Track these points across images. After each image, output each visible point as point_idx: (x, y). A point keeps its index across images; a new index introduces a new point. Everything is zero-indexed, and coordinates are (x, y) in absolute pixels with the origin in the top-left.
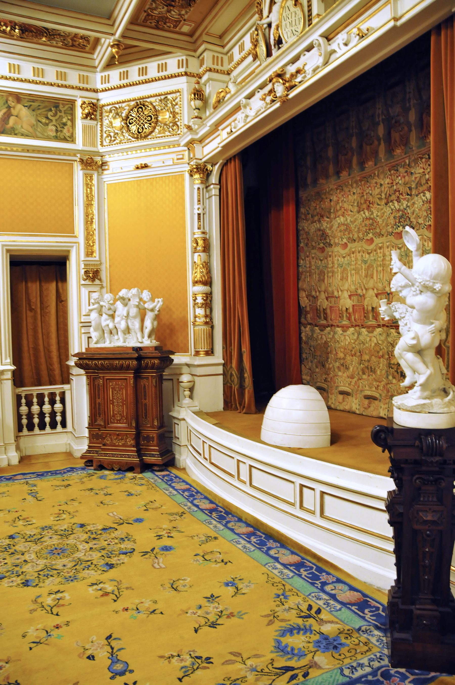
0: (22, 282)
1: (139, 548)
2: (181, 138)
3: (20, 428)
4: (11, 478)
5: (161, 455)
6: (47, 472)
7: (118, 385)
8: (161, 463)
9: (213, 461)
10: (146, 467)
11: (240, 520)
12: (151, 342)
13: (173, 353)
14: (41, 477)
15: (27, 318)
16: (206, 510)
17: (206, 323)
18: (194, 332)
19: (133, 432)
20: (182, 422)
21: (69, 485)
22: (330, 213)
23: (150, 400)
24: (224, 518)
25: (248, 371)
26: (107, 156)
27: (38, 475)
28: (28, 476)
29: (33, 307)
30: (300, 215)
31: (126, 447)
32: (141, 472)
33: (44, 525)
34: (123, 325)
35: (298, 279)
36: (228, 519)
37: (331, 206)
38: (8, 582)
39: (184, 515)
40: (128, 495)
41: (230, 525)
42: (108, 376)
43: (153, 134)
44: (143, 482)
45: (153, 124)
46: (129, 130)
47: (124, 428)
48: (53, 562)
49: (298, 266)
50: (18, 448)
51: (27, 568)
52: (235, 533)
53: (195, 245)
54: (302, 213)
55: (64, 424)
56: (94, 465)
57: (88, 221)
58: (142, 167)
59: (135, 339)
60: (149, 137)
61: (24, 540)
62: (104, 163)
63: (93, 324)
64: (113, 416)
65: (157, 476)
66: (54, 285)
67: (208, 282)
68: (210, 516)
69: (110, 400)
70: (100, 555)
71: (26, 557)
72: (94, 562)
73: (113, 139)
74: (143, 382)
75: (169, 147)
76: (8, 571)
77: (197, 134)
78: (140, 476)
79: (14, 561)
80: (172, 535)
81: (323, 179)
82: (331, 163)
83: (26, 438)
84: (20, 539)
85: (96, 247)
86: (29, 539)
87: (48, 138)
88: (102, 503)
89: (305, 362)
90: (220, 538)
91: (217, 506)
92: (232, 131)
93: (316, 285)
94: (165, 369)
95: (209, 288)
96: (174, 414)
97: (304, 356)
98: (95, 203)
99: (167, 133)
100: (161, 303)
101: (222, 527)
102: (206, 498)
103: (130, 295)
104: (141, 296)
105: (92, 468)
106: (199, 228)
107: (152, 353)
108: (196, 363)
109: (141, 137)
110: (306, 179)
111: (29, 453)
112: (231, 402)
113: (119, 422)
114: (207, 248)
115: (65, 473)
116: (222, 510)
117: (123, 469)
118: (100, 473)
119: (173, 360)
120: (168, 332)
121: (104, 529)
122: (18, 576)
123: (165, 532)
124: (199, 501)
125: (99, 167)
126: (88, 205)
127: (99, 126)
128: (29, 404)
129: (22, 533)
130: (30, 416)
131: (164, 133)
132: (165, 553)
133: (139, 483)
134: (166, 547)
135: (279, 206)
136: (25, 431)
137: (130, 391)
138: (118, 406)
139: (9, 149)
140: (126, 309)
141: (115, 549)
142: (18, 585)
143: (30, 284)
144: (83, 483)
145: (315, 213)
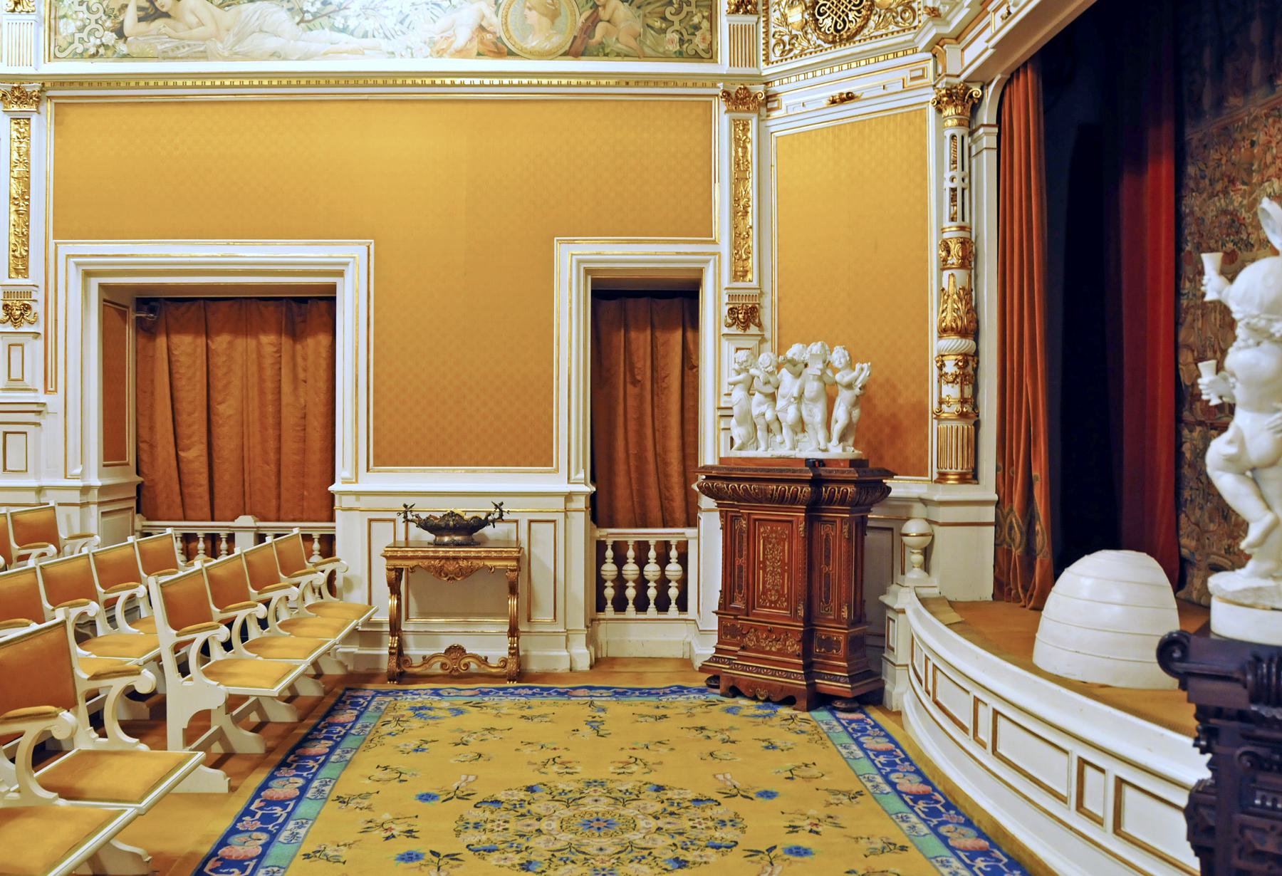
0: (619, 330)
1: (746, 842)
2: (917, 35)
3: (600, 605)
4: (566, 693)
5: (852, 679)
6: (634, 690)
7: (776, 532)
8: (850, 696)
9: (939, 698)
10: (820, 700)
11: (969, 823)
12: (844, 450)
13: (890, 475)
14: (623, 698)
15: (627, 397)
16: (907, 794)
17: (962, 415)
18: (941, 432)
19: (799, 627)
20: (901, 616)
21: (665, 716)
22: (1250, 172)
23: (836, 567)
24: (939, 814)
25: (1042, 518)
26: (777, 83)
27: (616, 693)
28: (597, 693)
29: (639, 378)
30: (1186, 181)
31: (784, 655)
32: (809, 710)
33: (593, 778)
34: (790, 415)
35: (1177, 324)
36: (945, 818)
37: (1253, 156)
38: (499, 860)
39: (860, 798)
40: (767, 748)
41: (943, 830)
42: (757, 514)
43: (865, 31)
44: (806, 727)
45: (864, 12)
46: (818, 27)
47: (783, 617)
48: (585, 841)
49: (1178, 293)
50: (591, 640)
51: (538, 843)
52: (948, 846)
53: (944, 254)
54: (1191, 178)
55: (683, 606)
56: (722, 685)
57: (739, 210)
58: (843, 101)
59: (814, 444)
60: (858, 38)
61: (550, 797)
62: (770, 98)
63: (736, 411)
64: (764, 593)
65: (838, 720)
66: (678, 335)
67: (971, 330)
68: (912, 808)
69: (759, 562)
70: (670, 841)
71: (543, 825)
72: (655, 853)
73: (788, 47)
74: (823, 530)
75: (896, 55)
76: (504, 842)
77: (948, 24)
78: (806, 715)
79: (519, 828)
80: (819, 829)
81: (1235, 96)
82: (1257, 58)
83: (611, 625)
84: (543, 794)
85: (752, 263)
86: (558, 797)
87: (666, 57)
88: (711, 754)
89: (1188, 509)
90: (913, 852)
91: (935, 789)
92: (1009, 13)
93: (1216, 337)
94: (871, 505)
95: (972, 343)
96: (887, 600)
97: (1186, 494)
98: (753, 175)
99: (892, 28)
100: (866, 373)
101: (925, 830)
102: (918, 772)
103: (806, 357)
104: (829, 358)
105: (718, 691)
106: (952, 219)
107: (843, 472)
108: (936, 498)
109: (841, 40)
110: (1200, 99)
111: (613, 653)
112: (1008, 584)
113: (773, 604)
114: (969, 259)
115: (665, 694)
116: (940, 798)
117: (775, 699)
118: (729, 702)
119: (889, 489)
120: (885, 435)
121: (696, 800)
122: (518, 852)
123: (808, 822)
124: (901, 775)
125: (760, 104)
126: (739, 179)
127: (762, 24)
128: (620, 561)
129: (551, 785)
130: (620, 583)
131: (886, 27)
132: (792, 858)
133: (798, 728)
134: (798, 848)
135: (1138, 161)
136: (609, 611)
137: (798, 546)
138: (773, 573)
139: (593, 82)
140: (798, 382)
141: (702, 836)
142: (514, 866)
143: (633, 334)
144: (691, 715)
145: (1218, 175)
